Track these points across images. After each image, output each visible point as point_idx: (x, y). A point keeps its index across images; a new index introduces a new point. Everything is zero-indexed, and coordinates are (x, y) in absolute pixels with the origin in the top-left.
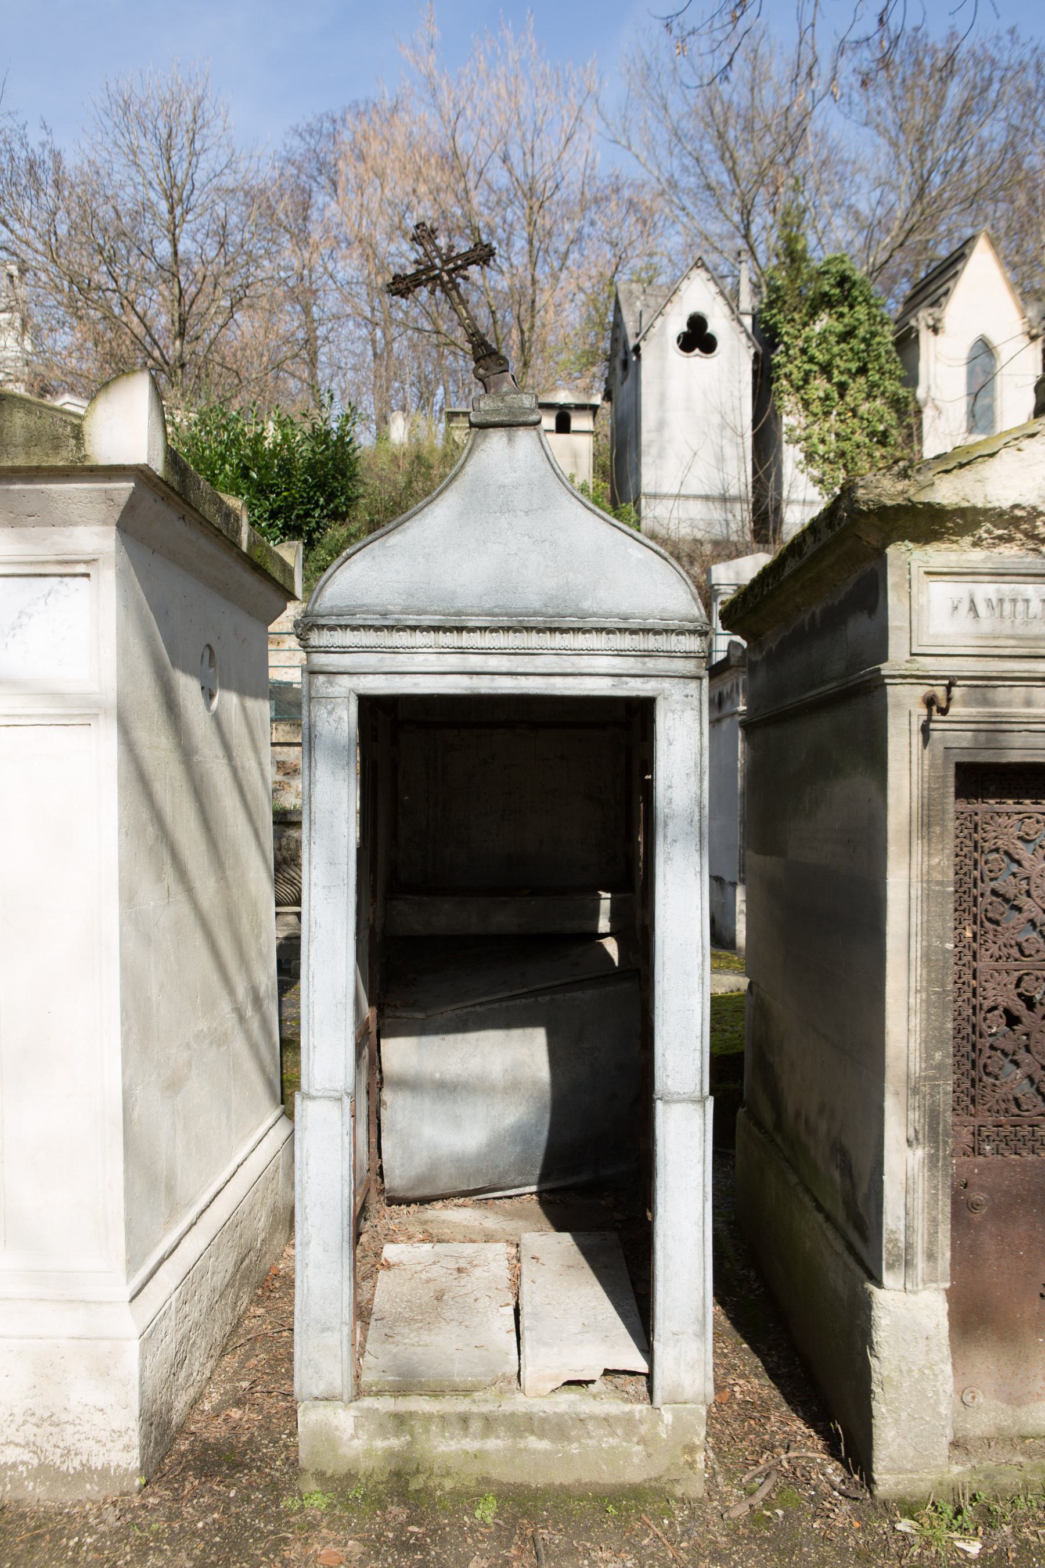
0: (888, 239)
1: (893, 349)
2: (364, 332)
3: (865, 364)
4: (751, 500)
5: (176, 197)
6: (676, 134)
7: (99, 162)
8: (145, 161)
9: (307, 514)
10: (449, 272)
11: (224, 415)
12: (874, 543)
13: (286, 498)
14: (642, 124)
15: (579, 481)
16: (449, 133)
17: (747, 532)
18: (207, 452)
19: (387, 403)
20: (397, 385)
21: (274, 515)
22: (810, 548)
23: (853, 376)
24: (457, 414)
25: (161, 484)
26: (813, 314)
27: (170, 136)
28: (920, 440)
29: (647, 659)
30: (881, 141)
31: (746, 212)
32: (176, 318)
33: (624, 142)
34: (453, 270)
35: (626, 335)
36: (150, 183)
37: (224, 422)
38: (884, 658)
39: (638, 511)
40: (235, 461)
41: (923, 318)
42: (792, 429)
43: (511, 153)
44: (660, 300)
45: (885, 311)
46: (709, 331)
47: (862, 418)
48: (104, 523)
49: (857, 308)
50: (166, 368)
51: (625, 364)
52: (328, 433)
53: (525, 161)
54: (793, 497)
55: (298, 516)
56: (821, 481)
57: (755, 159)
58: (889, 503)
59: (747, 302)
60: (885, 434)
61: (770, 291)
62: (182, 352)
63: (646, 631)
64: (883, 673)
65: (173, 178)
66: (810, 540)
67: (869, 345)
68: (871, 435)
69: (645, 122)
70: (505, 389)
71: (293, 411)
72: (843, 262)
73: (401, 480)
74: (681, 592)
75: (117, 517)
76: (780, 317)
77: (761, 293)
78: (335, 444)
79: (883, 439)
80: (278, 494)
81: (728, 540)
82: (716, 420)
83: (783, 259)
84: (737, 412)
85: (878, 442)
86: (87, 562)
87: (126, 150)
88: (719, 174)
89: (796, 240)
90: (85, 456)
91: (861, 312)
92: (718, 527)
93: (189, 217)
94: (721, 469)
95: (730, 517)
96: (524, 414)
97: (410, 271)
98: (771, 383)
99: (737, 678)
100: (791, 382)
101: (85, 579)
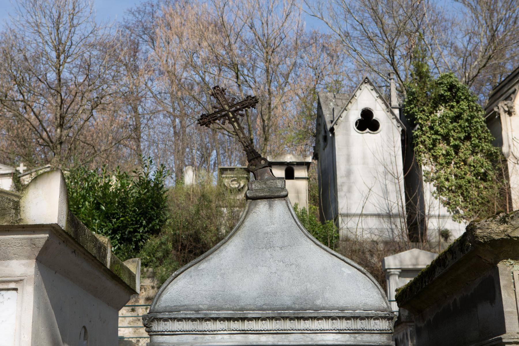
0: (476, 63)
1: (485, 125)
2: (169, 121)
3: (469, 134)
4: (406, 216)
5: (60, 49)
6: (349, 11)
7: (16, 31)
8: (44, 31)
9: (135, 231)
10: (233, 113)
11: (86, 172)
12: (489, 260)
13: (122, 221)
14: (328, 6)
15: (300, 207)
16: (220, 14)
17: (405, 235)
18: (75, 194)
19: (183, 161)
20: (187, 150)
21: (115, 231)
22: (450, 262)
23: (463, 141)
24: (226, 169)
25: (64, 234)
26: (435, 107)
27: (59, 17)
28: (508, 178)
29: (357, 335)
30: (467, 10)
31: (392, 52)
32: (58, 116)
33: (319, 15)
34: (235, 111)
35: (325, 122)
36: (46, 42)
37: (85, 176)
38: (503, 331)
39: (337, 225)
40: (92, 200)
41: (501, 106)
42: (428, 173)
43: (255, 23)
44: (344, 101)
45: (477, 103)
46: (374, 118)
47: (470, 165)
48: (29, 258)
49: (461, 103)
50: (51, 145)
51: (325, 138)
52: (149, 182)
53: (263, 28)
54: (432, 213)
55: (130, 232)
56: (448, 204)
57: (394, 24)
58: (496, 238)
59: (395, 101)
60: (485, 174)
61: (408, 95)
62: (61, 135)
63: (355, 318)
64: (504, 341)
65: (60, 40)
66: (449, 257)
67: (470, 123)
68: (477, 175)
69: (331, 5)
70: (266, 177)
71: (127, 169)
72: (451, 77)
73: (193, 209)
74: (375, 294)
75: (37, 255)
76: (416, 109)
77: (403, 96)
78: (153, 188)
79: (484, 177)
80: (117, 219)
81: (394, 241)
82: (381, 169)
83: (415, 77)
84: (394, 164)
85: (481, 179)
86: (16, 282)
87: (33, 24)
88: (373, 28)
89: (423, 67)
90: (20, 219)
91: (464, 105)
92: (387, 233)
93: (69, 60)
94: (386, 198)
95: (394, 226)
96: (278, 191)
97: (211, 111)
98: (414, 147)
99: (406, 329)
100: (425, 146)
101: (14, 292)
